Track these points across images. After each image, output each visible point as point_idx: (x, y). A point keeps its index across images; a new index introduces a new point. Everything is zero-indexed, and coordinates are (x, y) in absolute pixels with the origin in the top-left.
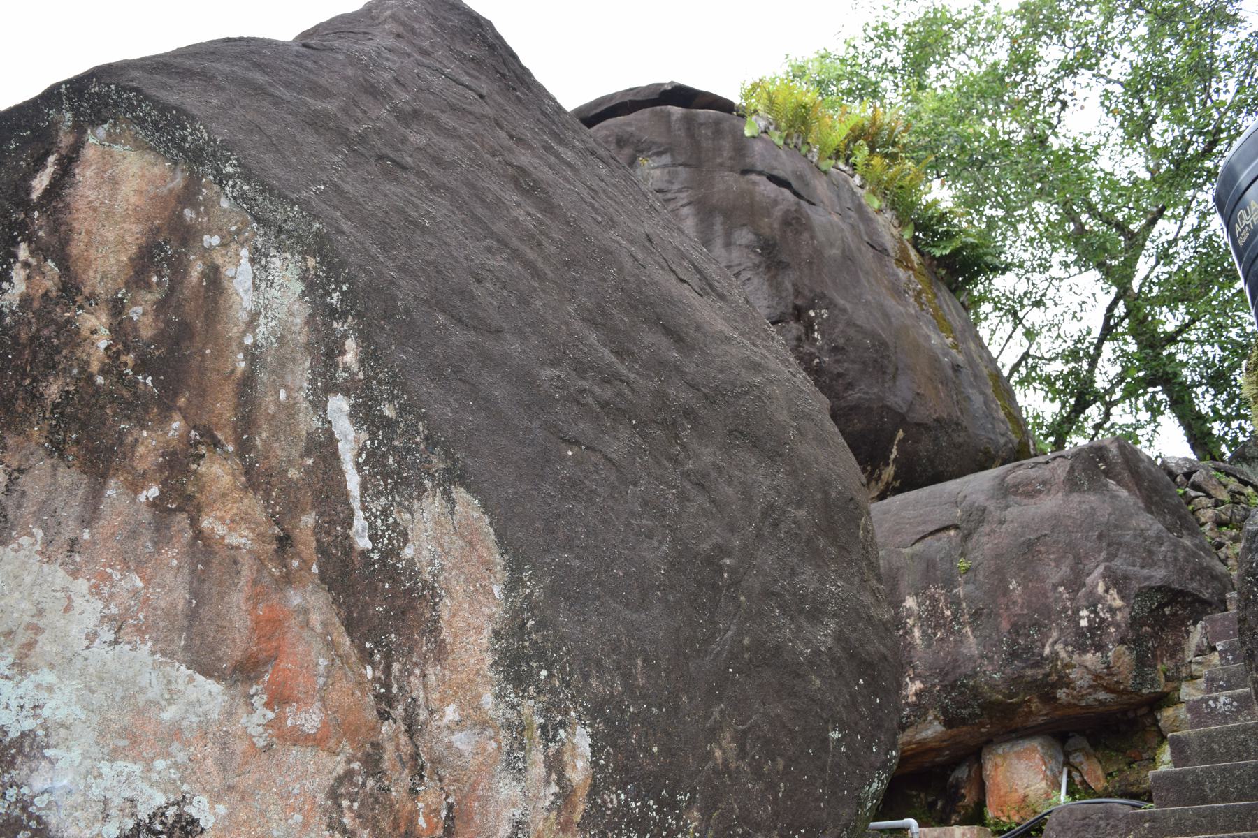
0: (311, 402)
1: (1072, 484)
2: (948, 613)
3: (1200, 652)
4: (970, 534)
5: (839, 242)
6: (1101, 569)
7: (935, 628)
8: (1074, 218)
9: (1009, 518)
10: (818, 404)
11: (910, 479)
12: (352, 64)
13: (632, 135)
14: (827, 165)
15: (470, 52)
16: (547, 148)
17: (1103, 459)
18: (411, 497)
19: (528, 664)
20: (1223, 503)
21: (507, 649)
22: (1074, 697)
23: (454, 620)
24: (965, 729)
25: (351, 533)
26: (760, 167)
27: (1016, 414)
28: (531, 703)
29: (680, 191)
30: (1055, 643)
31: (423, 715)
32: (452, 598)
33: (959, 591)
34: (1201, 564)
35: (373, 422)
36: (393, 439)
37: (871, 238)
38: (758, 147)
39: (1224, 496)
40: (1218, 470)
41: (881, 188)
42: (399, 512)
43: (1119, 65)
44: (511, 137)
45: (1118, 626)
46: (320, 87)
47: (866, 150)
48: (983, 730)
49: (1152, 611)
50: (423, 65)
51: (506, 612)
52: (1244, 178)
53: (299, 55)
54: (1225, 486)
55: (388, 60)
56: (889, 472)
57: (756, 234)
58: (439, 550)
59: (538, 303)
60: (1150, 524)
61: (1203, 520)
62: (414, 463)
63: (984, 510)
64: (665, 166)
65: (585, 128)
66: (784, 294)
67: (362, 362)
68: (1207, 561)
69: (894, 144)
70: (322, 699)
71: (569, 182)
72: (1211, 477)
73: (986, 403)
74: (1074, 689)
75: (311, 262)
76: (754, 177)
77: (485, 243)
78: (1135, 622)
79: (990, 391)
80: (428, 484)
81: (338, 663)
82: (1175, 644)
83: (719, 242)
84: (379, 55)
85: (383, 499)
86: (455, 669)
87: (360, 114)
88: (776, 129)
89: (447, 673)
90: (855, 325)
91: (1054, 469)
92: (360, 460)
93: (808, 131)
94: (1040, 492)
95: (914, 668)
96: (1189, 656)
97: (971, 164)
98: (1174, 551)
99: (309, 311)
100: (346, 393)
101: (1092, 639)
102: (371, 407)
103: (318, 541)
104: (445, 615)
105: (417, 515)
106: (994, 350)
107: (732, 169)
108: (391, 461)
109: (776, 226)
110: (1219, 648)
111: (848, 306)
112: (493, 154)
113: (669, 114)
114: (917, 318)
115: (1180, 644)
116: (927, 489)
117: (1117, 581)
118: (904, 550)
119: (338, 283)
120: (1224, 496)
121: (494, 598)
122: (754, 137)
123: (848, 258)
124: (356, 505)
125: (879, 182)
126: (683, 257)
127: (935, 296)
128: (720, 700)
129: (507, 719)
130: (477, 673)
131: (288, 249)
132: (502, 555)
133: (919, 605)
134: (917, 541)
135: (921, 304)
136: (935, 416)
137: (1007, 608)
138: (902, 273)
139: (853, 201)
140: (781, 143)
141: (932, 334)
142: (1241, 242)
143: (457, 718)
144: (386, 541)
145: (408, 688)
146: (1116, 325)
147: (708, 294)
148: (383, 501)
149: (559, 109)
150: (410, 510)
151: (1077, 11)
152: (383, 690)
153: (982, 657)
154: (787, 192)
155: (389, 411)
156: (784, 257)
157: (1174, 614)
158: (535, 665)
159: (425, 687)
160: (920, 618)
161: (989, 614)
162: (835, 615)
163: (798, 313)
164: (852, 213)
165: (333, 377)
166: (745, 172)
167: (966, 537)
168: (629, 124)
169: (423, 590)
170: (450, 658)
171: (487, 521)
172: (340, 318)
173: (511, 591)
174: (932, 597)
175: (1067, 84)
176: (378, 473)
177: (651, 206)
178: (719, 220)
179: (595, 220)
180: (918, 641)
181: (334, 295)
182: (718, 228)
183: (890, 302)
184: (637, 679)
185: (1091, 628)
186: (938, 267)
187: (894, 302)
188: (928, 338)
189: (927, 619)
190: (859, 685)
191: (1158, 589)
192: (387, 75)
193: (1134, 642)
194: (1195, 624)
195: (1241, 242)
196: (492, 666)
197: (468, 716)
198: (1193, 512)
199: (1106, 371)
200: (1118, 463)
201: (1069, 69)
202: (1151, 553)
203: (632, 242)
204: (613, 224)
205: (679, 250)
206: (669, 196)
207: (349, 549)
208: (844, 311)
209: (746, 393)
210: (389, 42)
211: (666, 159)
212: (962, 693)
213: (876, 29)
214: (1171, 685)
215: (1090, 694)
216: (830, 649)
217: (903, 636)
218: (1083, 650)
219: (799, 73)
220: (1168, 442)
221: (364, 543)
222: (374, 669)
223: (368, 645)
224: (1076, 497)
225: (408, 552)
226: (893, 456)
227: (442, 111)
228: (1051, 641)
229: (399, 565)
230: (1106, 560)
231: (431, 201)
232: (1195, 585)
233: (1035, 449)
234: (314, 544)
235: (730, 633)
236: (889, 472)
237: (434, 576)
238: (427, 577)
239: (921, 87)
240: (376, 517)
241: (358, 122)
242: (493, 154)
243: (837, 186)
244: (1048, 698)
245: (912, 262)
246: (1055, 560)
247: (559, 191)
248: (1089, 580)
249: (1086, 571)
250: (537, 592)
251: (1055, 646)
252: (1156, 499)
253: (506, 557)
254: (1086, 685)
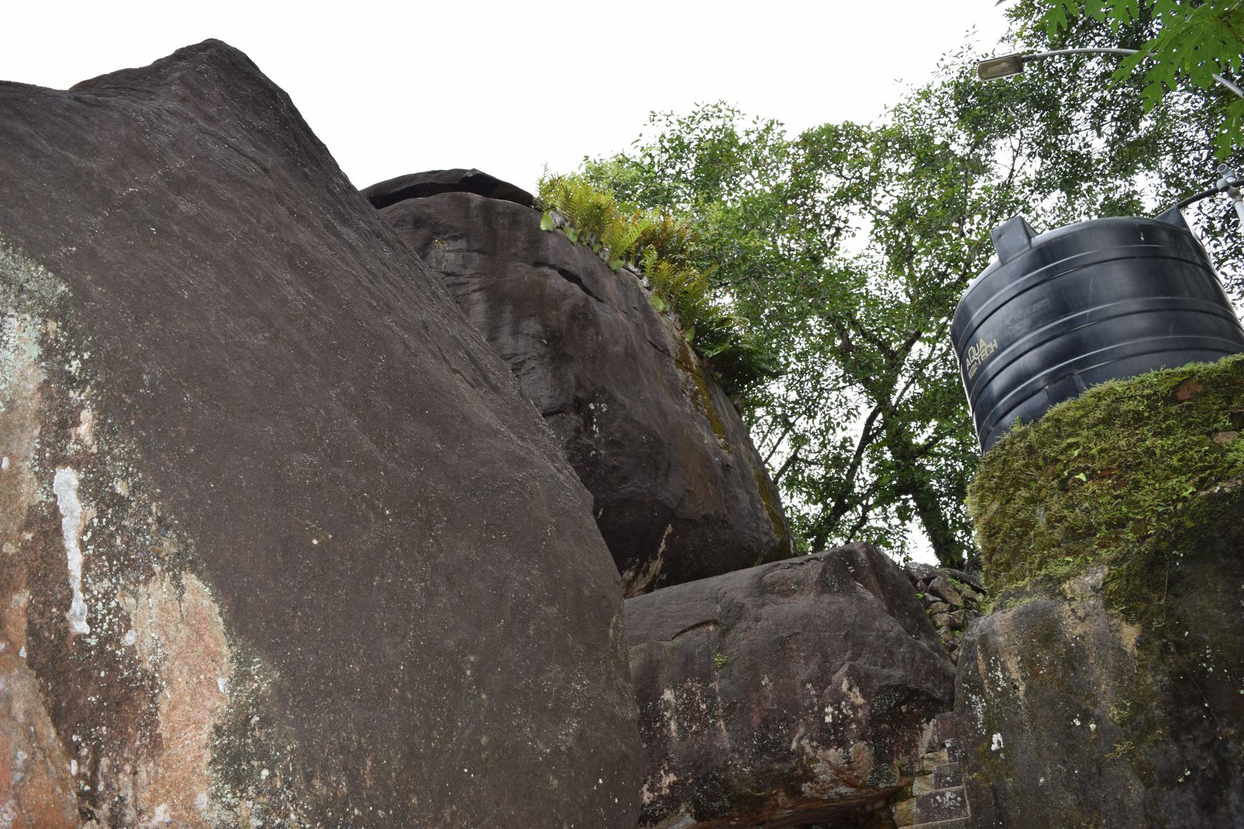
0: (36, 473)
1: (824, 586)
2: (704, 707)
3: (932, 748)
4: (728, 630)
5: (623, 340)
6: (845, 668)
7: (690, 721)
8: (843, 334)
9: (764, 616)
10: (578, 498)
11: (676, 574)
12: (127, 124)
13: (430, 217)
14: (617, 264)
15: (260, 124)
16: (329, 227)
17: (853, 562)
18: (138, 581)
19: (248, 762)
20: (957, 608)
21: (228, 746)
22: (817, 791)
23: (173, 713)
24: (715, 822)
25: (67, 615)
26: (552, 261)
27: (779, 514)
28: (250, 804)
29: (472, 276)
30: (801, 738)
31: (130, 815)
32: (173, 690)
33: (715, 685)
34: (935, 665)
35: (103, 498)
36: (123, 518)
37: (653, 338)
38: (552, 241)
39: (958, 601)
40: (954, 577)
41: (666, 291)
42: (123, 596)
43: (887, 198)
44: (292, 213)
45: (858, 722)
46: (89, 143)
47: (655, 254)
48: (732, 823)
49: (890, 709)
50: (207, 133)
51: (230, 707)
52: (976, 317)
53: (69, 108)
54: (960, 592)
55: (168, 123)
56: (656, 566)
57: (544, 326)
58: (163, 638)
59: (298, 386)
60: (891, 626)
61: (939, 623)
62: (143, 544)
63: (742, 607)
64: (459, 251)
65: (373, 209)
66: (566, 386)
67: (96, 436)
68: (941, 662)
69: (682, 251)
70: (17, 797)
71: (348, 264)
72: (947, 584)
73: (751, 503)
74: (817, 783)
75: (52, 326)
76: (546, 270)
77: (248, 320)
78: (874, 720)
79: (756, 492)
80: (157, 568)
81: (40, 756)
82: (910, 741)
83: (506, 331)
84: (159, 117)
85: (106, 581)
86: (170, 766)
87: (128, 178)
88: (571, 226)
89: (161, 770)
90: (632, 420)
91: (808, 570)
92: (85, 538)
93: (601, 231)
94: (794, 591)
95: (669, 760)
96: (922, 751)
97: (749, 273)
98: (912, 652)
99: (44, 377)
100: (77, 466)
101: (834, 735)
102: (102, 483)
103: (30, 622)
104: (164, 708)
105: (143, 600)
106: (764, 452)
107: (525, 260)
108: (118, 541)
109: (563, 319)
110: (948, 745)
111: (627, 402)
112: (269, 230)
113: (469, 200)
114: (693, 418)
115: (914, 741)
116: (691, 584)
117: (860, 680)
118: (664, 643)
119: (79, 351)
120: (958, 601)
121: (218, 691)
122: (549, 231)
123: (630, 355)
124: (76, 585)
125: (665, 286)
126: (459, 346)
127: (711, 397)
128: (451, 802)
129: (222, 821)
130: (193, 771)
131: (29, 310)
132: (230, 646)
133: (677, 698)
134: (678, 634)
135: (697, 405)
136: (703, 513)
137: (759, 703)
138: (680, 373)
139: (639, 302)
140: (575, 240)
141: (705, 434)
142: (971, 376)
143: (168, 819)
144: (106, 626)
145: (116, 786)
146: (874, 435)
147: (480, 385)
148: (106, 583)
149: (351, 188)
150: (135, 595)
151: (854, 146)
152: (87, 788)
153: (733, 751)
154: (576, 287)
155: (121, 488)
156: (569, 350)
157: (910, 712)
158: (255, 763)
159: (135, 784)
160: (677, 711)
161: (742, 709)
162: (578, 714)
163: (579, 406)
164: (637, 313)
165: (63, 449)
166: (538, 264)
167: (724, 633)
168: (428, 206)
169: (142, 680)
170: (165, 754)
171: (217, 610)
172: (77, 387)
173: (238, 685)
174: (689, 691)
175: (841, 212)
176: (103, 554)
177: (433, 293)
178: (509, 308)
179: (370, 304)
180: (674, 734)
181: (74, 363)
182: (507, 315)
183: (668, 401)
184: (364, 780)
185: (834, 724)
186: (716, 370)
187: (671, 400)
188: (701, 437)
189: (684, 712)
190: (598, 785)
191: (896, 688)
192: (163, 139)
193: (873, 738)
194: (928, 722)
195: (971, 376)
196: (210, 764)
197: (180, 817)
198: (931, 616)
199: (865, 476)
200: (868, 567)
201: (844, 196)
202: (891, 653)
203: (407, 329)
204: (389, 309)
205: (456, 339)
206: (462, 280)
207: (64, 632)
208: (623, 406)
209: (508, 487)
210: (172, 105)
211: (461, 244)
212: (713, 786)
213: (671, 141)
214: (905, 780)
215: (832, 788)
216: (569, 749)
217: (660, 728)
218: (827, 745)
219: (597, 174)
220: (918, 549)
221: (81, 627)
222: (79, 764)
223: (75, 738)
224: (826, 598)
225: (129, 639)
226: (661, 550)
227: (219, 181)
228: (798, 736)
229: (118, 652)
230: (850, 659)
231: (195, 272)
232: (929, 685)
233: (795, 549)
234: (24, 627)
235: (467, 732)
236: (656, 566)
237: (155, 665)
238: (148, 666)
239: (709, 199)
240: (97, 600)
241: (125, 185)
242: (269, 230)
243: (626, 286)
244: (794, 792)
245: (691, 364)
246: (805, 658)
247: (336, 273)
248: (835, 678)
249: (832, 669)
250: (264, 687)
251: (801, 741)
252: (898, 602)
253: (234, 649)
254: (829, 779)
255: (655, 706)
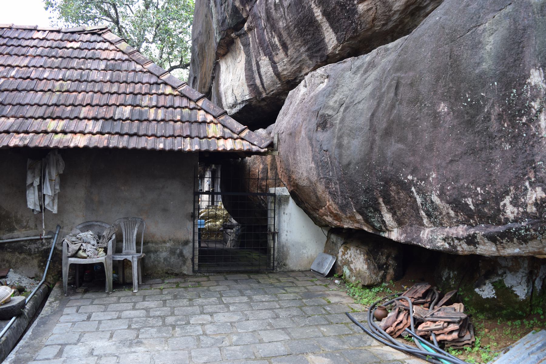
255: (520, 94)
